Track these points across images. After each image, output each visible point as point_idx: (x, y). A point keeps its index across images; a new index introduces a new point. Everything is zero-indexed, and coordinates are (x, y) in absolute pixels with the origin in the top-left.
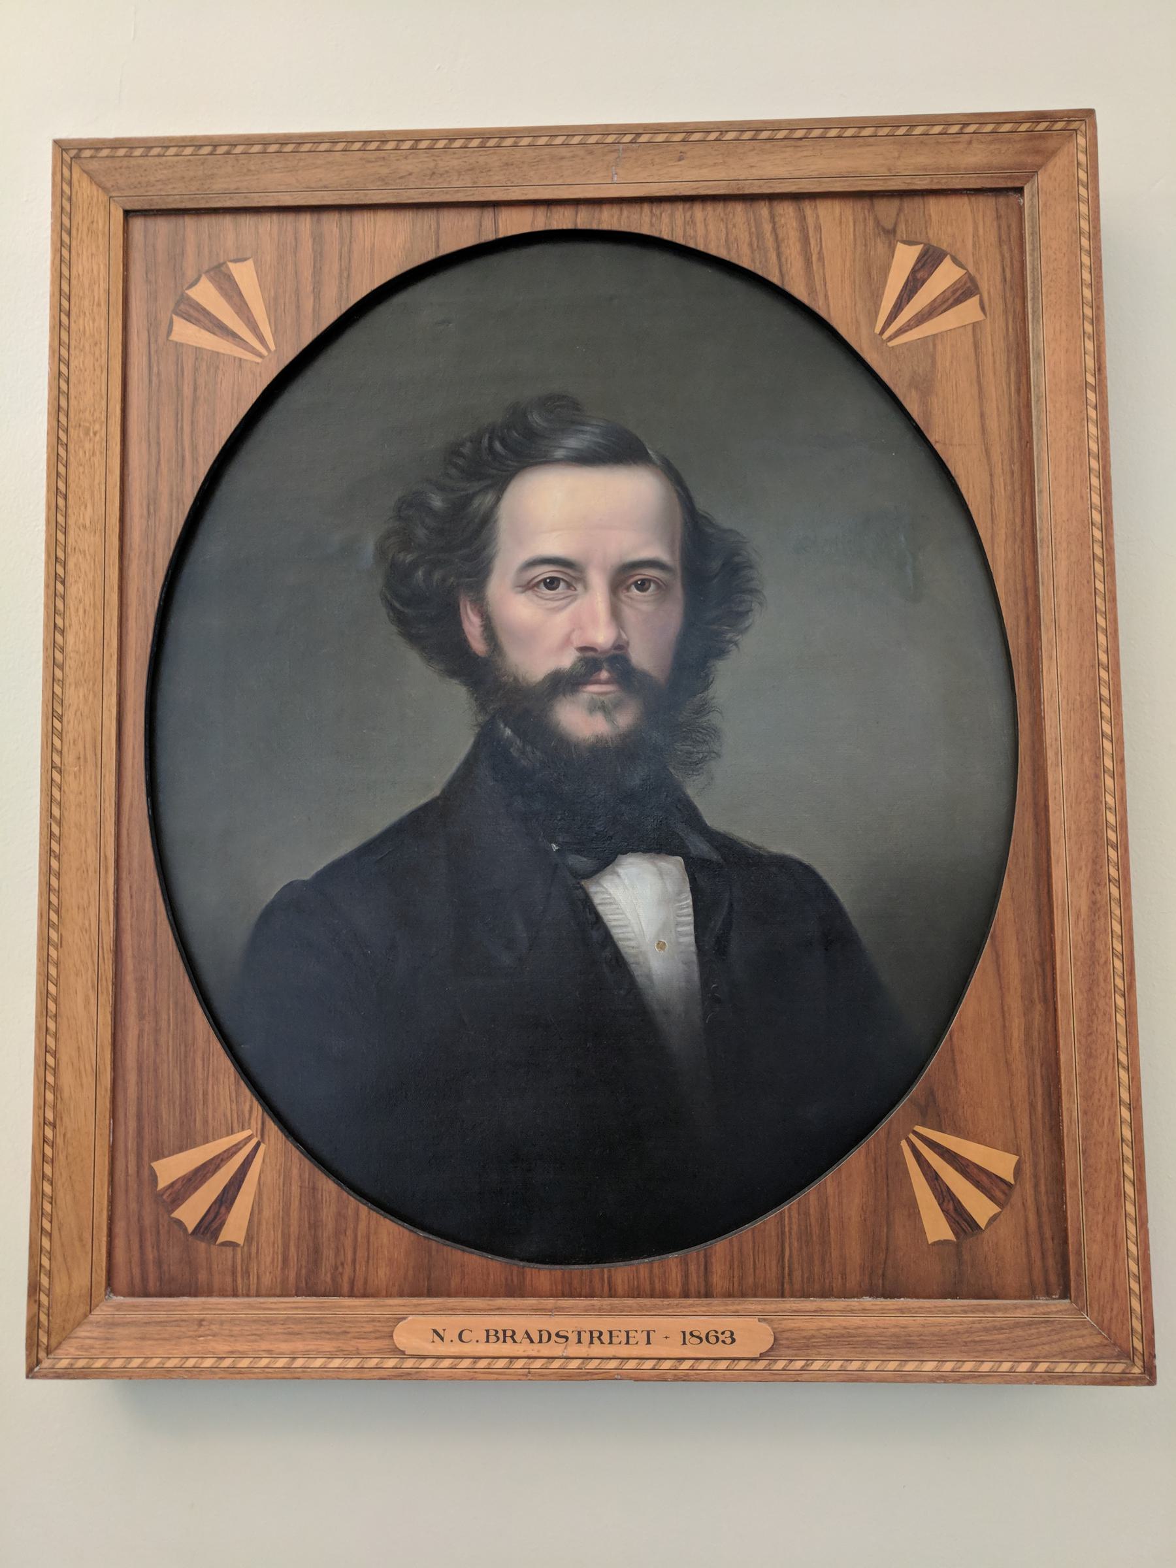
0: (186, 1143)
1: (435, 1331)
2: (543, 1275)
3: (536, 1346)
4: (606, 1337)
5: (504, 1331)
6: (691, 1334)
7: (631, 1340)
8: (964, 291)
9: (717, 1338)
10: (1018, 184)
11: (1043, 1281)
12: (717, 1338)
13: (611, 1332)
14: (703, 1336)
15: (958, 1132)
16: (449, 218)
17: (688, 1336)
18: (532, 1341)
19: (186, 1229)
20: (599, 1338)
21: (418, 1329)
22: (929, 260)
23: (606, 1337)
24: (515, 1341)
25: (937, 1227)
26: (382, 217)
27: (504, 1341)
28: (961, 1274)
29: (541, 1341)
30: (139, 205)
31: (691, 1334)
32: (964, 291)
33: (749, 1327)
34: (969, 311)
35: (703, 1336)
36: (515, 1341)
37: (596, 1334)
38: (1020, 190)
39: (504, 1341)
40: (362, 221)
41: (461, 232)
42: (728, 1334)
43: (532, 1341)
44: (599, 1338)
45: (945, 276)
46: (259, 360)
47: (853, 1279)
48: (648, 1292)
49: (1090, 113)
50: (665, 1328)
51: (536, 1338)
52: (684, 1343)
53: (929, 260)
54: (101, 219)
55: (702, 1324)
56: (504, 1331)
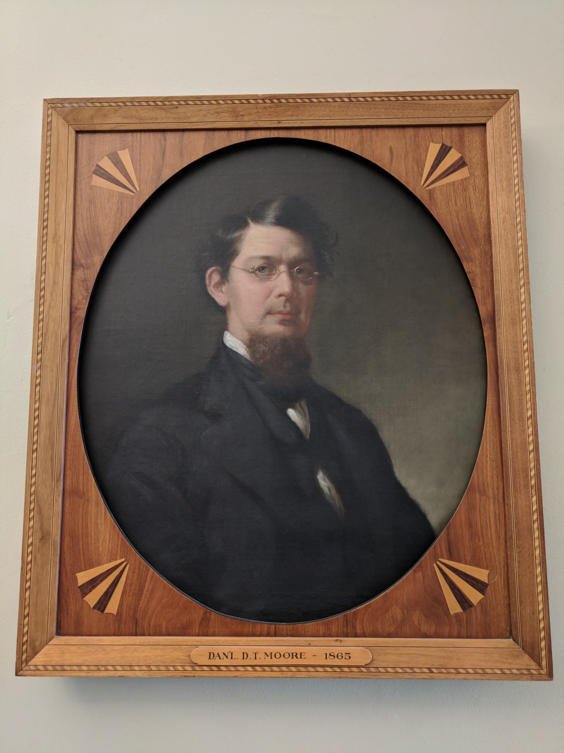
0: (90, 565)
1: (266, 653)
2: (265, 626)
3: (299, 659)
4: (299, 656)
5: (292, 654)
6: (330, 655)
9: (342, 657)
10: (483, 122)
11: (508, 619)
13: (301, 653)
15: (459, 561)
16: (234, 133)
17: (328, 655)
18: (220, 658)
21: (201, 647)
23: (299, 656)
24: (297, 658)
25: (454, 607)
26: (108, 136)
27: (293, 658)
28: (472, 624)
29: (243, 658)
30: (80, 123)
31: (330, 655)
33: (356, 649)
36: (297, 658)
37: (294, 654)
38: (484, 125)
39: (293, 658)
40: (187, 134)
41: (221, 141)
43: (220, 658)
44: (296, 656)
45: (452, 157)
47: (164, 630)
48: (273, 634)
49: (518, 91)
51: (229, 657)
52: (326, 658)
56: (292, 654)
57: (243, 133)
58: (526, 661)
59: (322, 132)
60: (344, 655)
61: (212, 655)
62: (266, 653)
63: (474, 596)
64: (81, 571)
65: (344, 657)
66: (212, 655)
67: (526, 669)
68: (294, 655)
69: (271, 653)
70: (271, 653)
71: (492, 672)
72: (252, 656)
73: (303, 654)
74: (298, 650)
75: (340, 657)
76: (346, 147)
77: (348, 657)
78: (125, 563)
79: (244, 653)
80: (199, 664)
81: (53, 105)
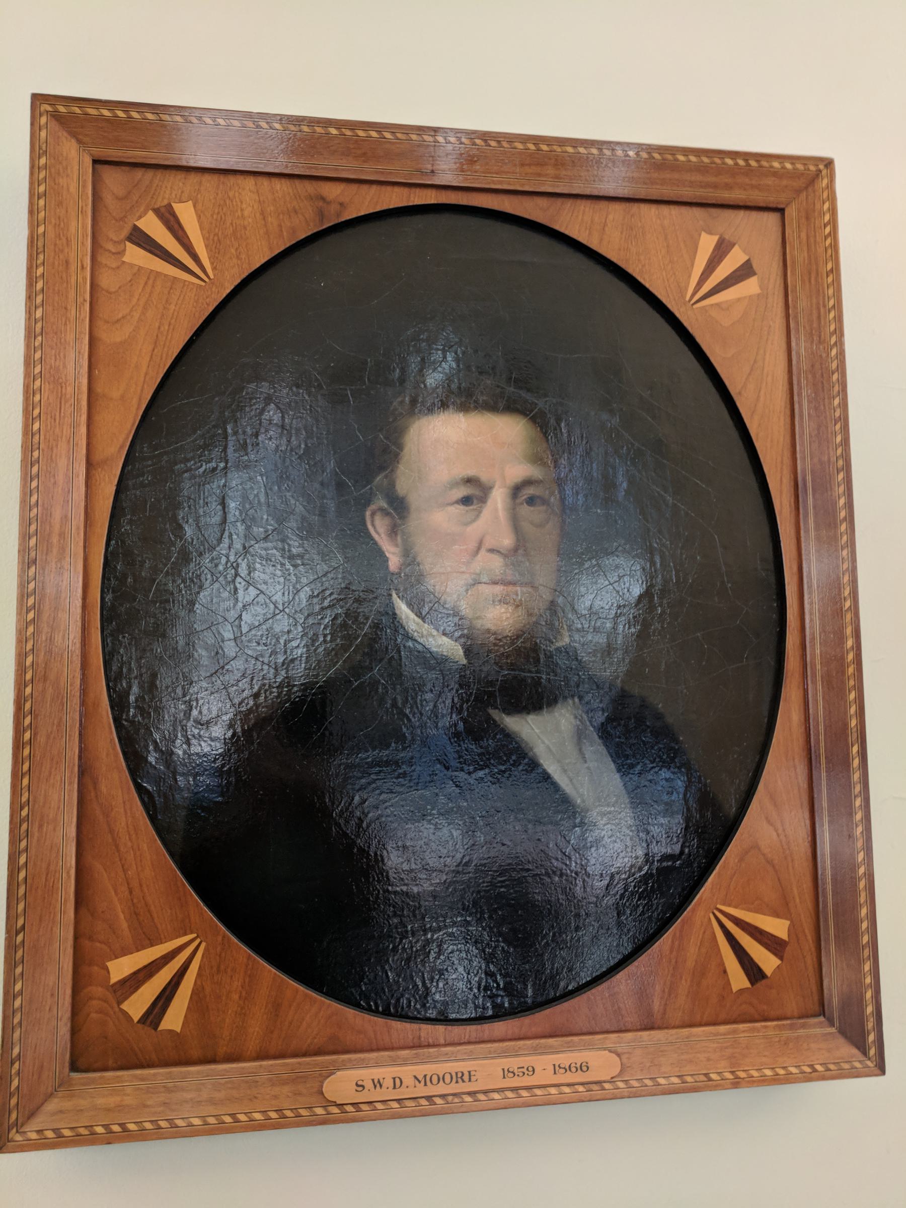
1: (415, 1077)
3: (468, 1083)
4: (466, 1078)
5: (457, 1073)
6: (509, 1071)
7: (473, 1078)
8: (745, 272)
11: (104, 149)
12: (527, 1069)
13: (469, 1072)
14: (567, 1067)
19: (132, 1020)
20: (461, 1077)
22: (721, 251)
23: (466, 1078)
24: (463, 1081)
25: (738, 980)
28: (758, 1002)
29: (394, 1088)
31: (509, 1071)
32: (745, 272)
33: (600, 1060)
34: (750, 287)
35: (567, 1067)
36: (463, 1081)
38: (781, 211)
42: (530, 1069)
46: (203, 284)
50: (545, 1063)
53: (721, 251)
54: (76, 158)
55: (564, 1059)
57: (405, 191)
58: (848, 1050)
59: (585, 208)
60: (516, 1071)
61: (398, 1081)
62: (415, 1077)
63: (767, 961)
64: (111, 960)
65: (526, 1072)
66: (398, 1081)
67: (229, 1115)
68: (459, 1077)
69: (425, 1076)
70: (425, 1076)
71: (696, 1077)
72: (369, 1085)
73: (472, 1073)
74: (463, 1066)
75: (574, 1069)
76: (584, 242)
77: (521, 1074)
78: (198, 941)
79: (394, 1079)
80: (338, 1102)
81: (829, 163)
